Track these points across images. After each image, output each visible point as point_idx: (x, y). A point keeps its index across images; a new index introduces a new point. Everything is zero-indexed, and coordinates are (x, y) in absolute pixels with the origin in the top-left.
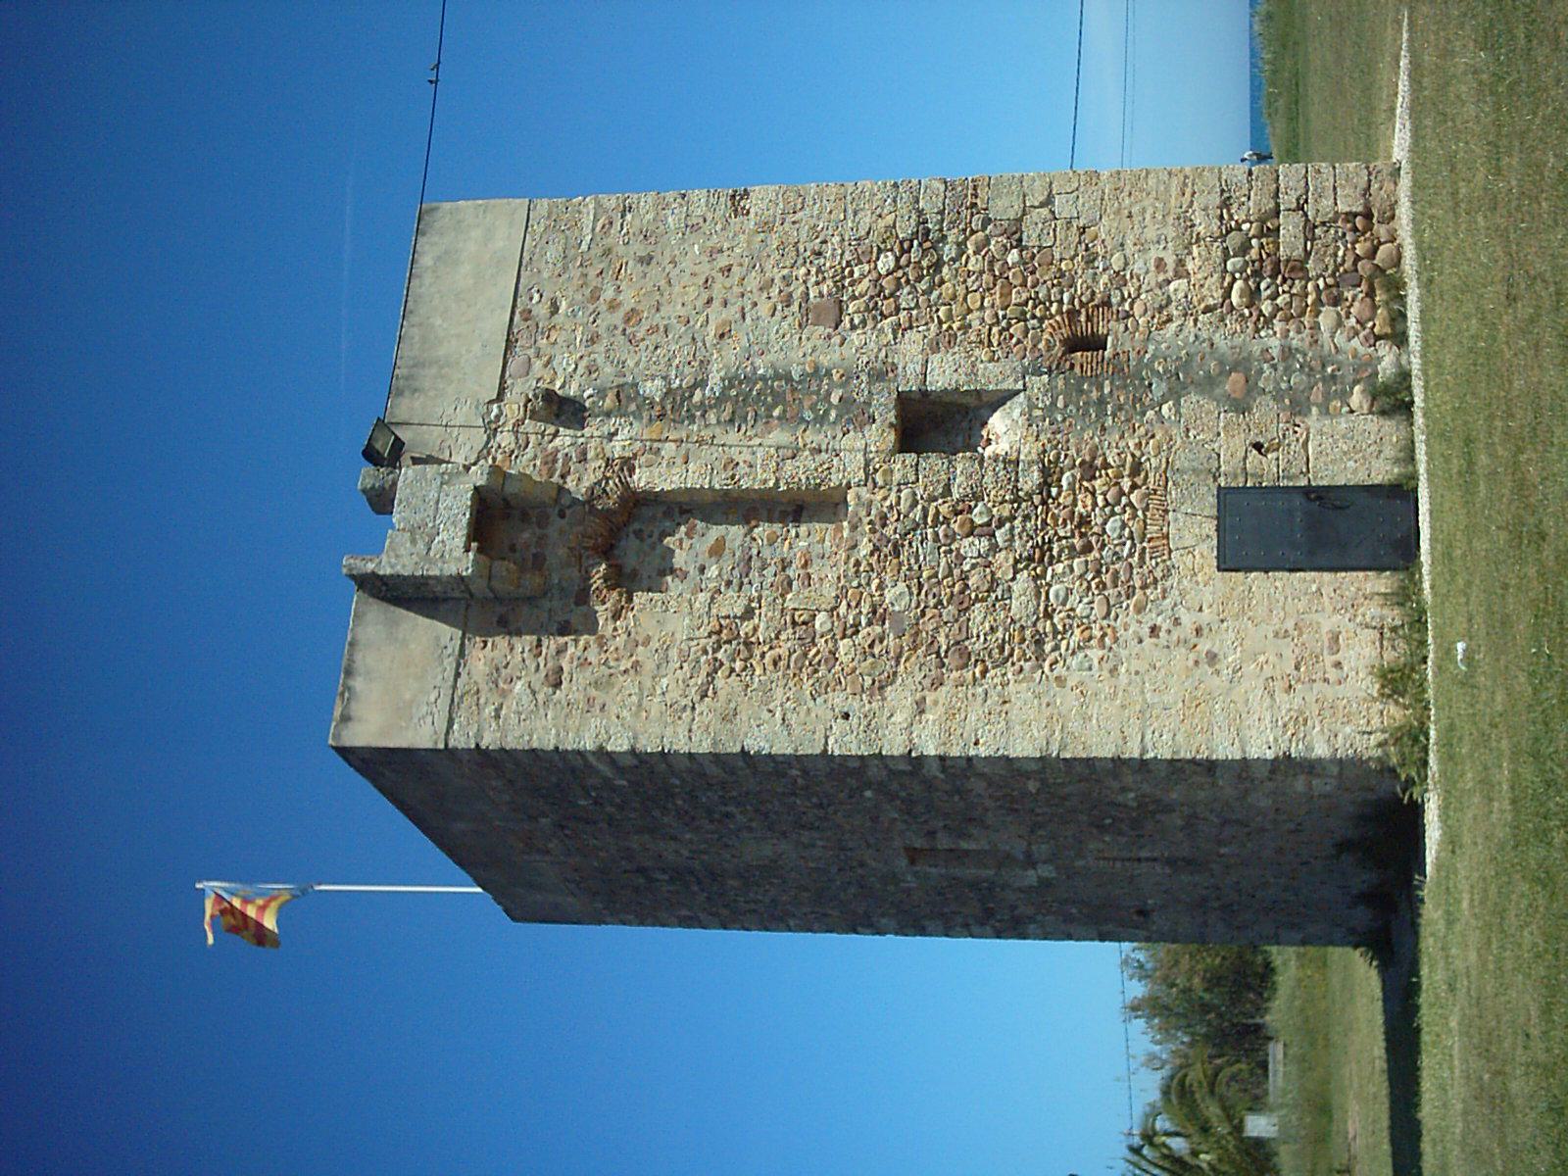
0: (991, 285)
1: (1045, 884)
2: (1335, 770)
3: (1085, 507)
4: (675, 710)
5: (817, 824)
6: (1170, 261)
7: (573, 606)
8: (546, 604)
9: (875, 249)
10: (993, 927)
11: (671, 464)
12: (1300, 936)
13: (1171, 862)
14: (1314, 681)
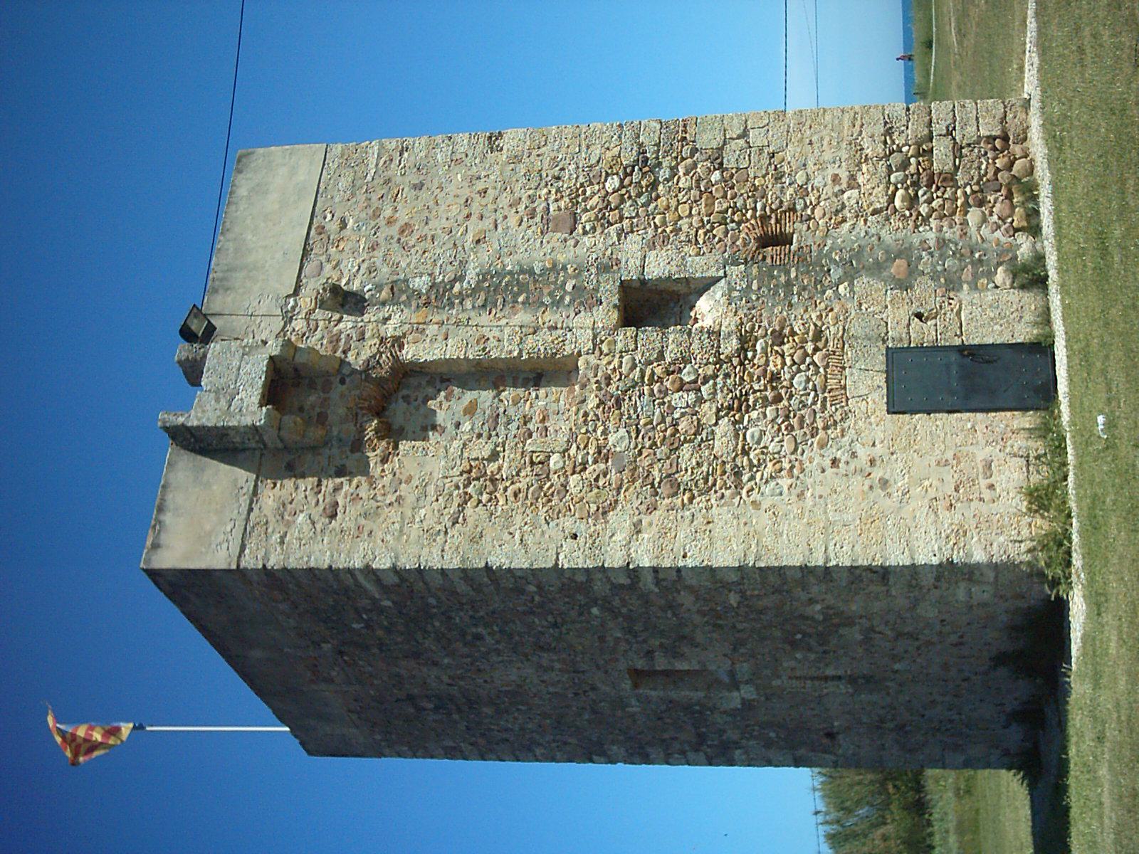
0: (698, 198)
2: (991, 575)
6: (844, 176)
7: (349, 453)
13: (852, 680)
14: (972, 500)
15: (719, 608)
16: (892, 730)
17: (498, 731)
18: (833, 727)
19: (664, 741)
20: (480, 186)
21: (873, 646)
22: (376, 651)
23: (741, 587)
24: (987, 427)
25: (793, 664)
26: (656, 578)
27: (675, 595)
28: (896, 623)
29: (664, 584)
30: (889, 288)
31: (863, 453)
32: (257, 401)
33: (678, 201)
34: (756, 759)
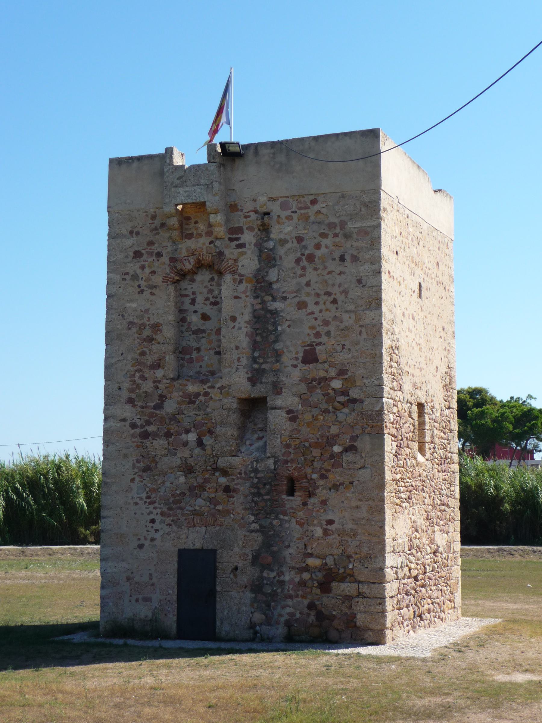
3: (209, 488)
7: (169, 257)
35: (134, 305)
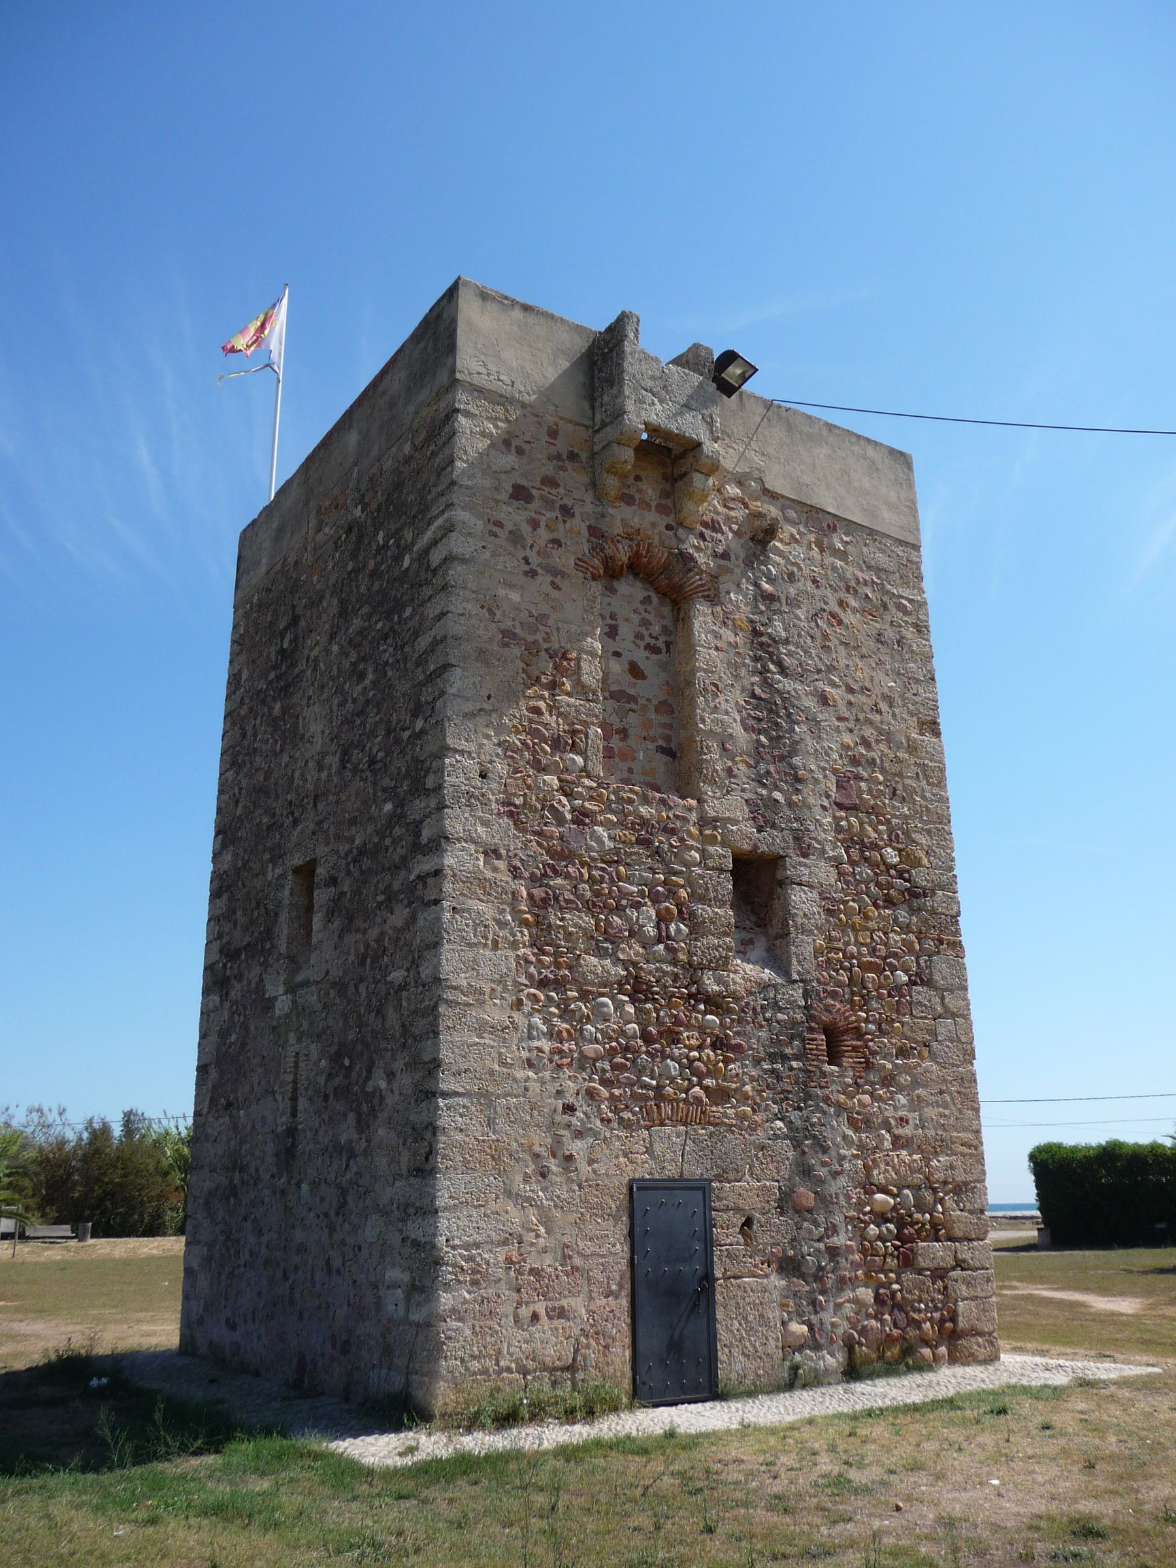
0: (878, 954)
1: (269, 1005)
2: (417, 1316)
4: (490, 607)
5: (348, 766)
6: (907, 1131)
7: (588, 523)
8: (589, 497)
9: (900, 846)
10: (217, 962)
11: (717, 636)
12: (195, 1266)
13: (292, 1132)
14: (519, 1291)
15: (386, 958)
16: (231, 1181)
17: (254, 725)
18: (239, 1109)
19: (234, 912)
20: (884, 706)
21: (331, 1157)
22: (350, 566)
23: (412, 984)
24: (612, 1311)
25: (314, 1056)
26: (428, 875)
27: (406, 902)
28: (358, 1186)
29: (420, 887)
30: (781, 1184)
31: (577, 1147)
32: (651, 419)
33: (874, 931)
34: (208, 1020)
35: (515, 597)
